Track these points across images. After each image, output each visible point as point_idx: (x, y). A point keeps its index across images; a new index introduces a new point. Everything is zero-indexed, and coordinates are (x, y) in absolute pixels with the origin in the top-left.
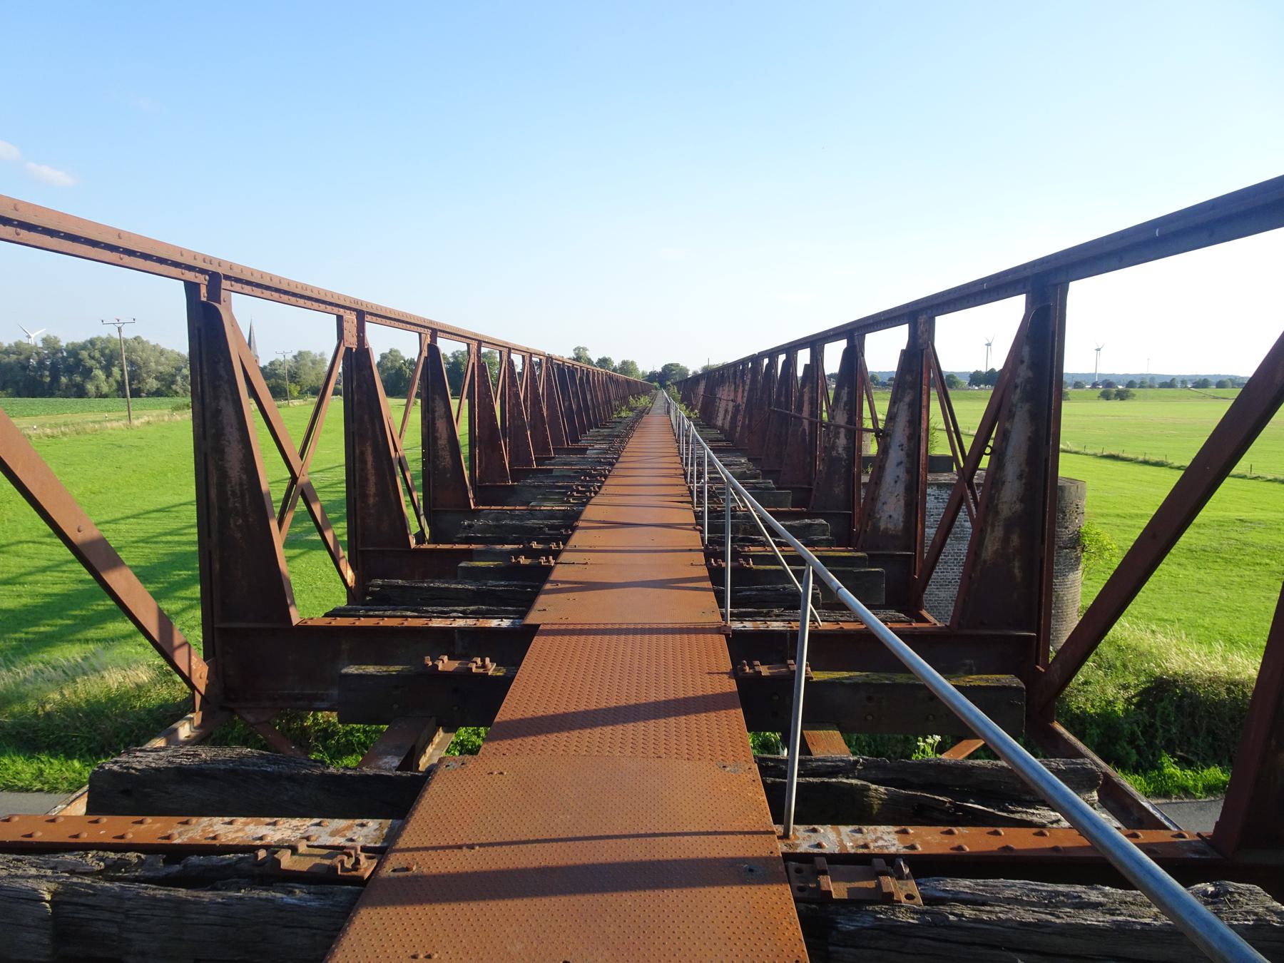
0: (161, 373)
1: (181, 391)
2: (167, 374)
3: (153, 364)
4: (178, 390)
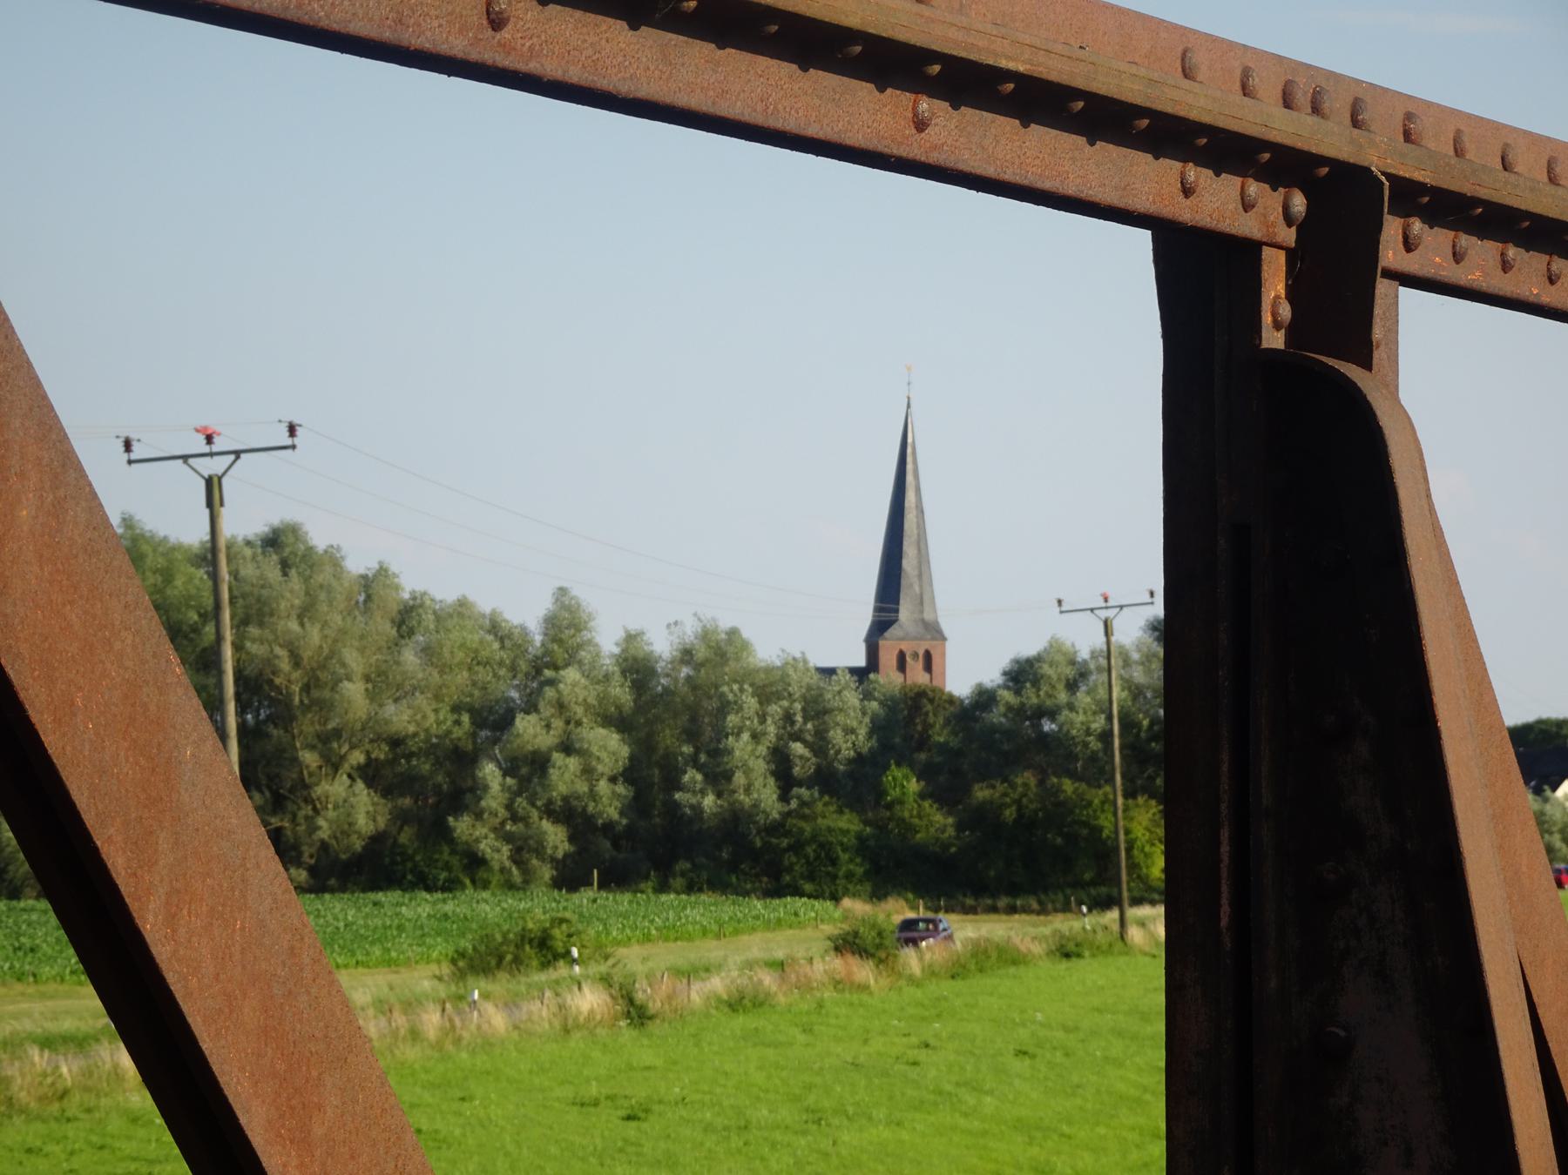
0: (396, 742)
1: (496, 852)
2: (430, 750)
3: (354, 691)
4: (486, 847)
